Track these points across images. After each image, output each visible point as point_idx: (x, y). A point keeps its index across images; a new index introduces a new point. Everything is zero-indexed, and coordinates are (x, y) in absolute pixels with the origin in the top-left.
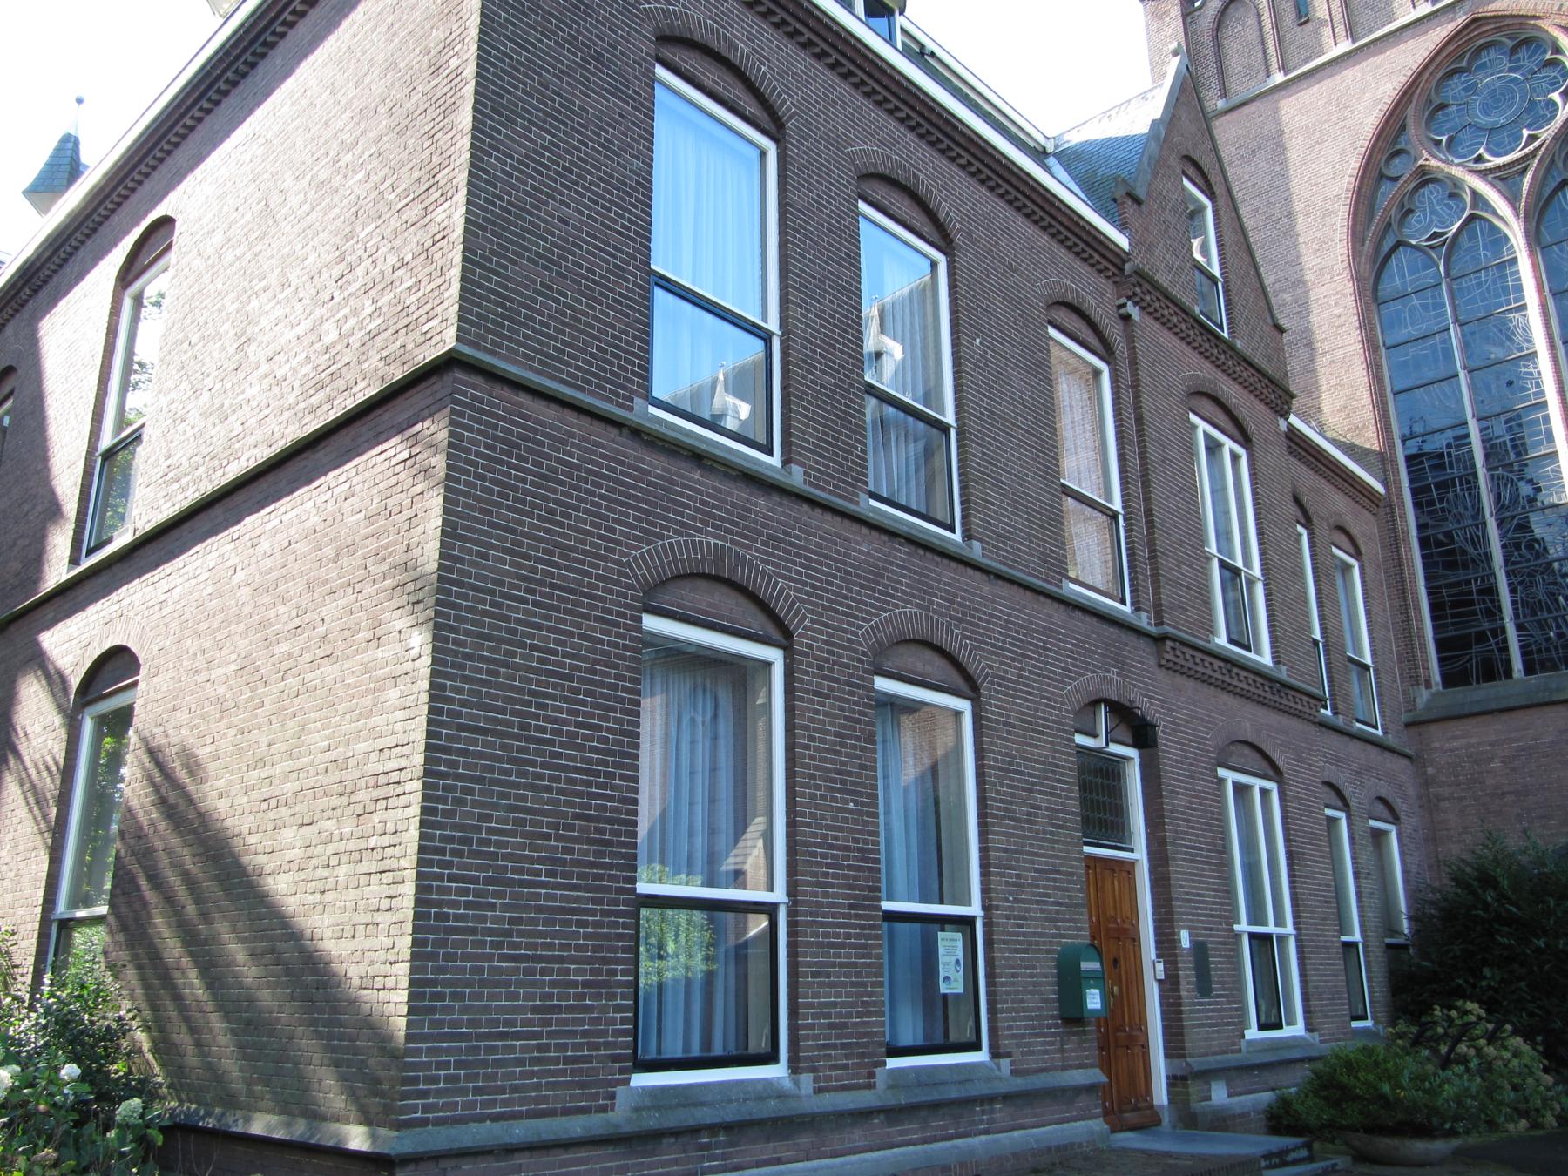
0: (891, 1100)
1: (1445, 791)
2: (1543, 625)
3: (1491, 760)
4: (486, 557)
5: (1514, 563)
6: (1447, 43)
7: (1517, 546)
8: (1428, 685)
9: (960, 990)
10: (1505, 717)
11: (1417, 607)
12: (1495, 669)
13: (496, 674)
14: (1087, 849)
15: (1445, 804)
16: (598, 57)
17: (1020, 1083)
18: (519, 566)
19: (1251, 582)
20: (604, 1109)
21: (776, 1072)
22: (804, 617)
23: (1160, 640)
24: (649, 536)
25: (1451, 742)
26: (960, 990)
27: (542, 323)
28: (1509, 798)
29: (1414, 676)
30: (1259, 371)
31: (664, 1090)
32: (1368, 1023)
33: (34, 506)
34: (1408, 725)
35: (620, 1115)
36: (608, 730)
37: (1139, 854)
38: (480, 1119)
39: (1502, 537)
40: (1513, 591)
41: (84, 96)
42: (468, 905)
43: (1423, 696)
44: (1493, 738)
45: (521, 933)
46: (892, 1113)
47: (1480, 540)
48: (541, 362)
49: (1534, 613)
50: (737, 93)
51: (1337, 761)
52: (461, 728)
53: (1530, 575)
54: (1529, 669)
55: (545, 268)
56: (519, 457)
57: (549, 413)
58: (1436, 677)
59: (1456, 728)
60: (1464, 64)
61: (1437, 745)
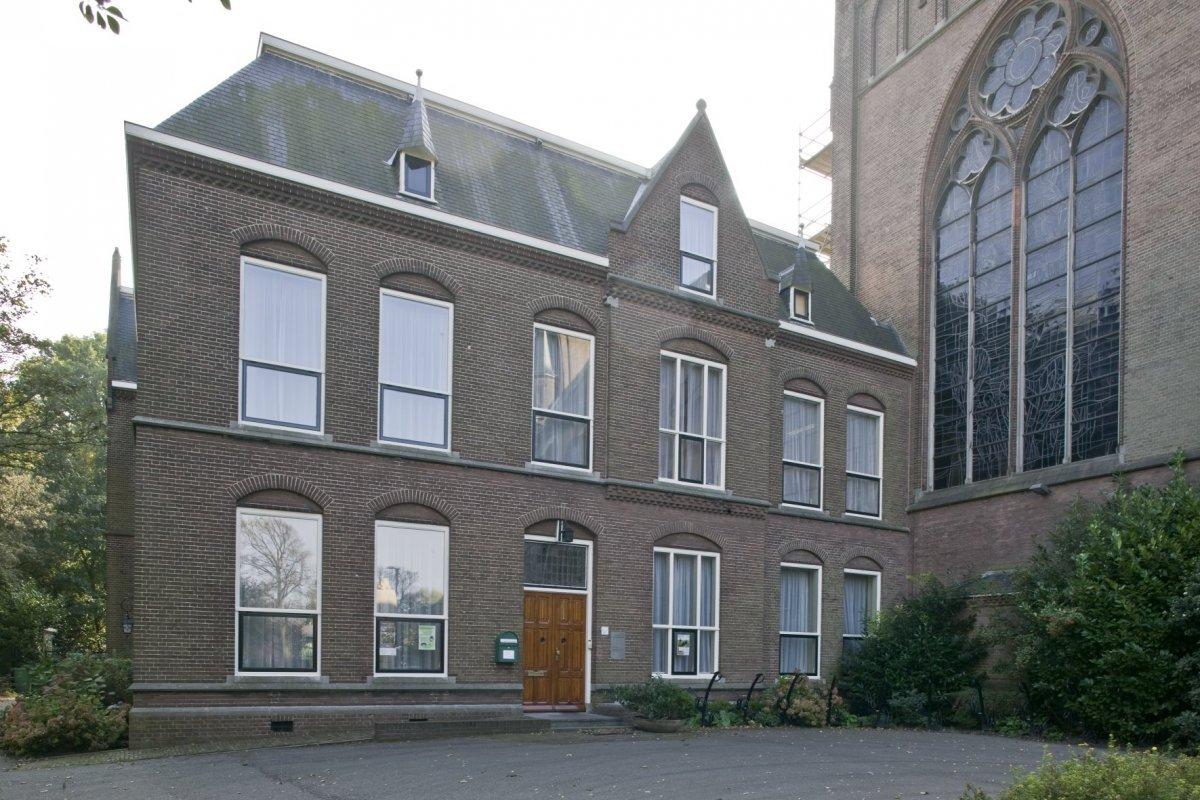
0: (373, 687)
1: (920, 552)
2: (985, 449)
3: (943, 534)
4: (156, 495)
5: (978, 410)
6: (998, 15)
7: (981, 398)
8: (924, 488)
9: (433, 648)
10: (953, 508)
11: (926, 439)
12: (959, 479)
13: (164, 537)
14: (526, 588)
15: (919, 560)
16: (206, 268)
17: (460, 686)
18: (173, 497)
19: (715, 446)
20: (221, 682)
21: (316, 675)
22: (330, 501)
23: (606, 485)
24: (239, 477)
25: (929, 522)
26: (433, 648)
27: (179, 399)
28: (948, 556)
29: (918, 481)
30: (734, 314)
31: (253, 677)
32: (818, 677)
33: (1157, 142)
34: (909, 513)
35: (227, 685)
36: (219, 554)
37: (589, 592)
38: (167, 682)
39: (975, 391)
40: (975, 428)
41: (415, 70)
42: (157, 616)
43: (920, 495)
44: (946, 520)
45: (181, 625)
46: (375, 693)
47: (963, 395)
48: (179, 415)
49: (982, 442)
50: (298, 255)
51: (816, 537)
52: (149, 557)
53: (985, 418)
54: (976, 478)
55: (180, 374)
56: (170, 456)
57: (185, 437)
58: (931, 483)
59: (931, 515)
60: (1007, 33)
61: (920, 525)
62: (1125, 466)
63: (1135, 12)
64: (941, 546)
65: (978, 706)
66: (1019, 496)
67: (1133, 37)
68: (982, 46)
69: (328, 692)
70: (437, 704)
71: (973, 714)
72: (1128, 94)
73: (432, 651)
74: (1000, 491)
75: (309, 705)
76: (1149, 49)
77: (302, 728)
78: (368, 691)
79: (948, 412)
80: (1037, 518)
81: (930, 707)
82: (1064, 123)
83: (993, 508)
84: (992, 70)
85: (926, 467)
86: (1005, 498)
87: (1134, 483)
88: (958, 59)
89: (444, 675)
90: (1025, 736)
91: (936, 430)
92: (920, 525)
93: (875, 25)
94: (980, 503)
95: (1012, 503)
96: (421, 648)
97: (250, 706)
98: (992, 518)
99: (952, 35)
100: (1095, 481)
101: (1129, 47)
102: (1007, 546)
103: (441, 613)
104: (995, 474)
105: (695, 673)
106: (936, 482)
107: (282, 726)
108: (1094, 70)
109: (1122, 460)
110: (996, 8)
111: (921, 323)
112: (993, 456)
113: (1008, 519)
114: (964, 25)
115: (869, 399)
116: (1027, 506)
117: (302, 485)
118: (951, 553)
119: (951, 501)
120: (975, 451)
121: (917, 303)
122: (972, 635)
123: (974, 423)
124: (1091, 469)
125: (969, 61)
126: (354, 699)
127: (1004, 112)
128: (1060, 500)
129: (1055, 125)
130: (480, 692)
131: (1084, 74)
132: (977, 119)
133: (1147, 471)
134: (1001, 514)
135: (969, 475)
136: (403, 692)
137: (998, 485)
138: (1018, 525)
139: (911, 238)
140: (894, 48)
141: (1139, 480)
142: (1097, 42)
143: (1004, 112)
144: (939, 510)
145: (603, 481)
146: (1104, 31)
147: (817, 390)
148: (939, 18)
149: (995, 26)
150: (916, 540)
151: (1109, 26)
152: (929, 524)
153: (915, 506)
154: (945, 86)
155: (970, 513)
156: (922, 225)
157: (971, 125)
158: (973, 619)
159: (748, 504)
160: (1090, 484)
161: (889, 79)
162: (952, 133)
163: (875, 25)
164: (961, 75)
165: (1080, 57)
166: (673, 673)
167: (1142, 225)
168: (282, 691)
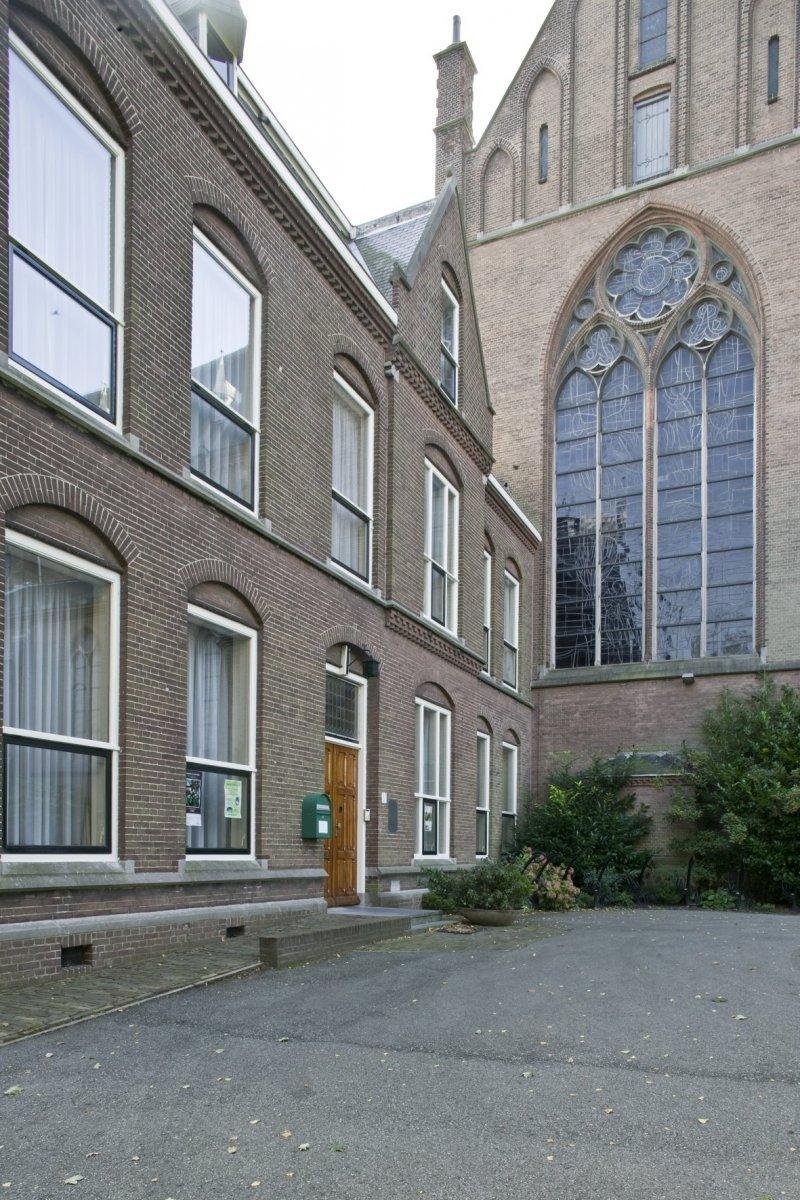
2: (615, 635)
3: (575, 713)
8: (548, 665)
11: (549, 616)
12: (585, 660)
15: (546, 737)
21: (111, 859)
22: (136, 552)
25: (555, 701)
28: (581, 736)
29: (541, 660)
31: (26, 865)
34: (533, 688)
39: (603, 577)
40: (603, 612)
43: (544, 672)
47: (590, 579)
51: (489, 704)
53: (614, 604)
54: (604, 661)
59: (559, 693)
61: (547, 701)
62: (767, 666)
63: (770, 269)
64: (573, 725)
65: (685, 883)
66: (659, 682)
67: (769, 290)
68: (613, 245)
69: (134, 890)
70: (250, 902)
71: (678, 890)
72: (765, 339)
73: (238, 820)
74: (642, 676)
75: (110, 913)
76: (784, 306)
77: (104, 957)
78: (181, 885)
79: (571, 592)
80: (681, 705)
81: (624, 886)
82: (698, 346)
83: (632, 692)
84: (619, 272)
85: (549, 645)
86: (645, 683)
87: (776, 681)
88: (588, 249)
89: (251, 858)
90: (736, 906)
91: (557, 609)
92: (547, 701)
93: (484, 179)
94: (617, 685)
95: (654, 689)
96: (227, 815)
97: (27, 920)
98: (630, 701)
99: (579, 223)
100: (739, 676)
101: (765, 298)
102: (647, 729)
103: (246, 763)
104: (626, 659)
105: (435, 853)
106: (557, 661)
107: (76, 954)
108: (725, 306)
109: (763, 660)
110: (629, 214)
111: (544, 499)
112: (624, 642)
113: (649, 703)
114: (594, 218)
115: (513, 565)
116: (668, 693)
117: (99, 515)
118: (585, 733)
119: (584, 681)
120: (603, 635)
121: (541, 477)
122: (632, 813)
123: (602, 608)
124: (734, 664)
125: (598, 257)
126: (164, 899)
127: (633, 317)
128: (703, 691)
129: (689, 345)
130: (291, 881)
131: (717, 309)
132: (606, 313)
133: (788, 673)
134: (642, 698)
135: (598, 658)
136: (218, 884)
137: (633, 670)
138: (659, 710)
139: (532, 411)
140: (509, 211)
141: (781, 680)
142: (727, 283)
143: (633, 317)
144: (568, 689)
145: (386, 603)
146: (734, 276)
147: (111, 558)
148: (564, 201)
149: (626, 231)
150: (541, 717)
151: (741, 271)
152: (558, 701)
153: (539, 683)
154: (572, 271)
155: (606, 695)
156: (546, 401)
157: (599, 318)
158: (632, 798)
159: (466, 653)
160: (733, 679)
161: (501, 241)
162: (575, 319)
163: (484, 179)
164: (591, 264)
165: (714, 291)
166: (424, 853)
167: (780, 457)
168: (74, 890)
